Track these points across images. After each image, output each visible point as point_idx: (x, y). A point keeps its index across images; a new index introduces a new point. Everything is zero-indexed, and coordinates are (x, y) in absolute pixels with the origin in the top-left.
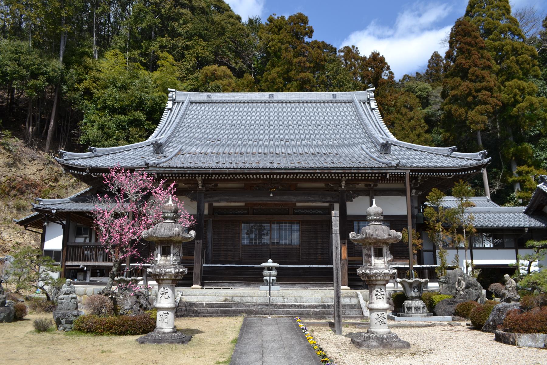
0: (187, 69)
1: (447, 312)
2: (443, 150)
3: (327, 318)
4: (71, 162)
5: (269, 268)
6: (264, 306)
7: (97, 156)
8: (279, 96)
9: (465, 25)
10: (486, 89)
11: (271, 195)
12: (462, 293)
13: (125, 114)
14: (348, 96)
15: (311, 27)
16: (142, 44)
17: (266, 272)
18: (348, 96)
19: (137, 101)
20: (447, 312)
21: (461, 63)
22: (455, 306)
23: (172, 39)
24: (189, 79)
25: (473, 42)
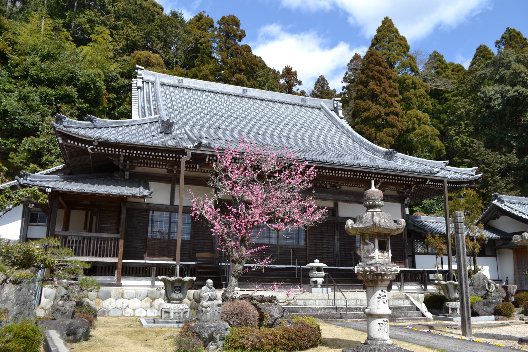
0: (117, 50)
1: (487, 312)
2: (437, 163)
3: (397, 321)
4: (73, 130)
5: (319, 269)
6: (331, 310)
7: (97, 128)
8: (252, 92)
9: (377, 56)
10: (393, 113)
11: (314, 192)
12: (493, 294)
13: (53, 88)
14: (316, 102)
15: (244, 32)
16: (67, 14)
17: (315, 273)
18: (316, 102)
19: (69, 75)
20: (487, 312)
21: (373, 89)
22: (493, 307)
23: (102, 15)
24: (117, 61)
25: (383, 71)
